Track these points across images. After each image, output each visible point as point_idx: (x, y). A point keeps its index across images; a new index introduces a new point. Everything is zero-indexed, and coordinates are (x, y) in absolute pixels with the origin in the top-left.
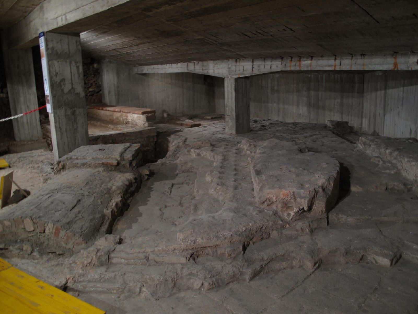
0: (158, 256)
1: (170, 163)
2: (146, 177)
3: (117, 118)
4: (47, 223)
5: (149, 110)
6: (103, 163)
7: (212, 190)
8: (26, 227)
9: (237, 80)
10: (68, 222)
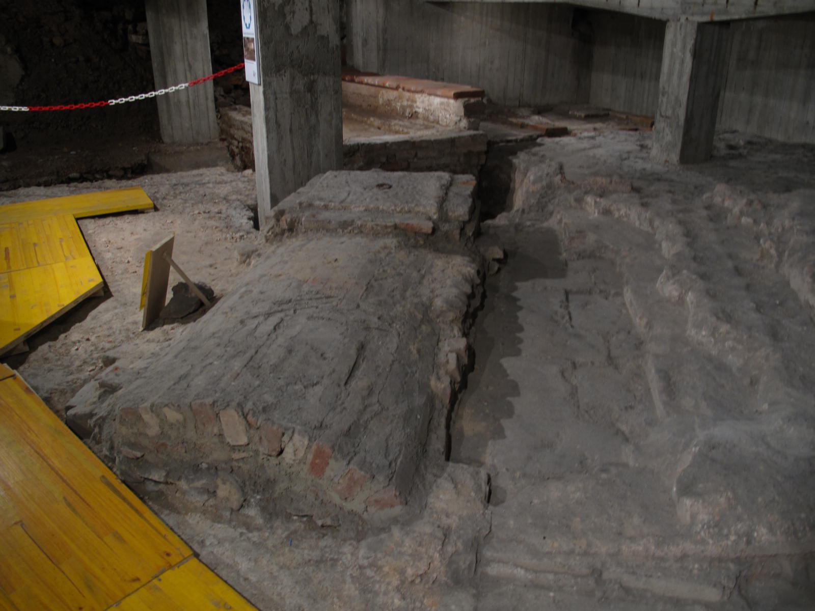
0: (634, 573)
1: (533, 225)
2: (496, 266)
3: (388, 103)
4: (290, 432)
5: (467, 88)
6: (396, 227)
7: (704, 333)
8: (227, 433)
9: (701, 26)
10: (346, 428)
